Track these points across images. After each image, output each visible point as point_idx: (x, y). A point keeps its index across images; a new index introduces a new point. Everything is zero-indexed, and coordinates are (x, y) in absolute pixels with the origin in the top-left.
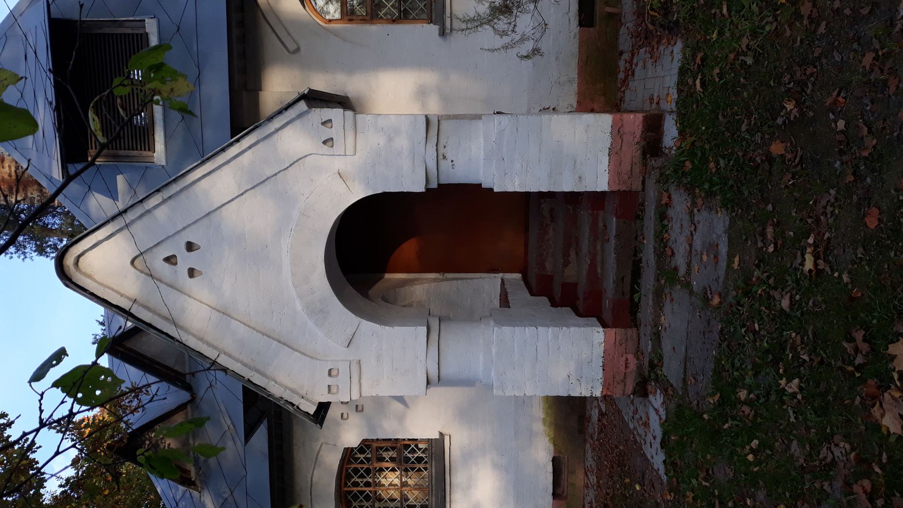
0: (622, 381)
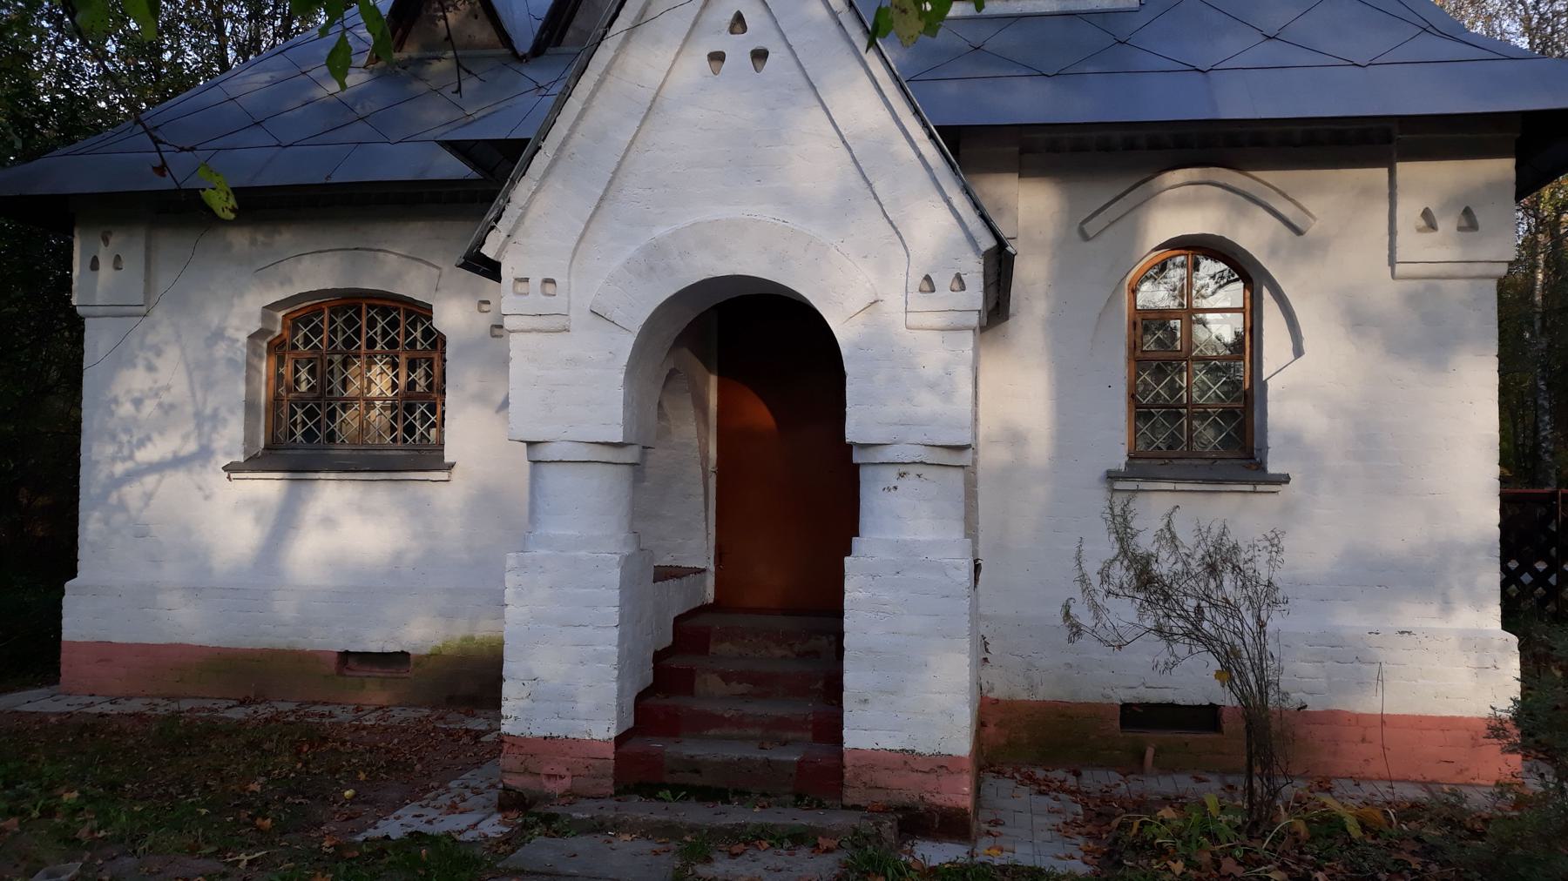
0: (526, 769)
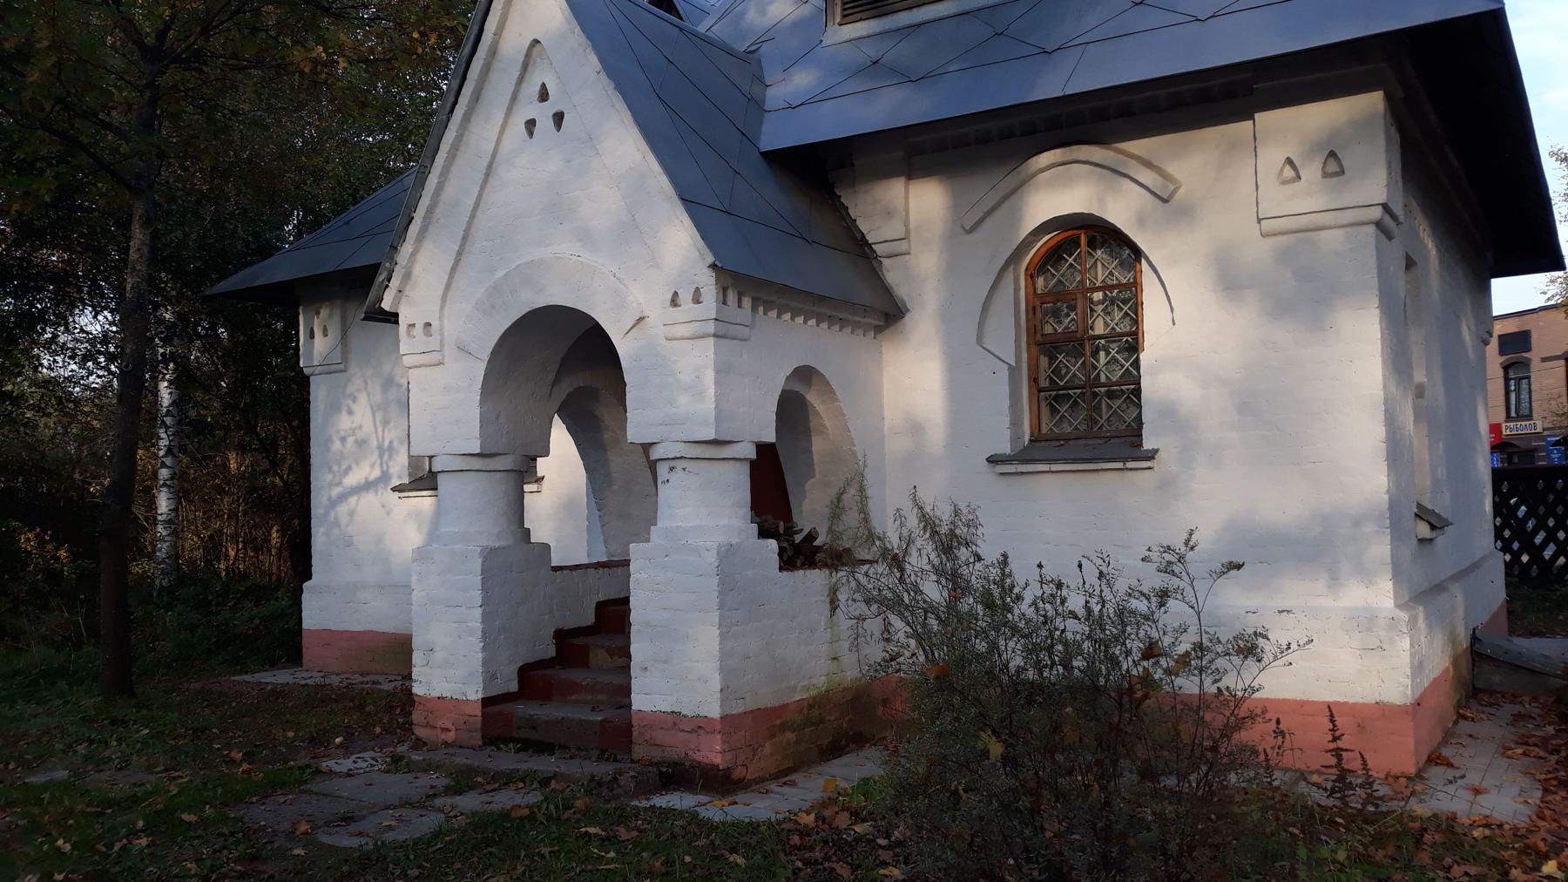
0: (428, 723)
